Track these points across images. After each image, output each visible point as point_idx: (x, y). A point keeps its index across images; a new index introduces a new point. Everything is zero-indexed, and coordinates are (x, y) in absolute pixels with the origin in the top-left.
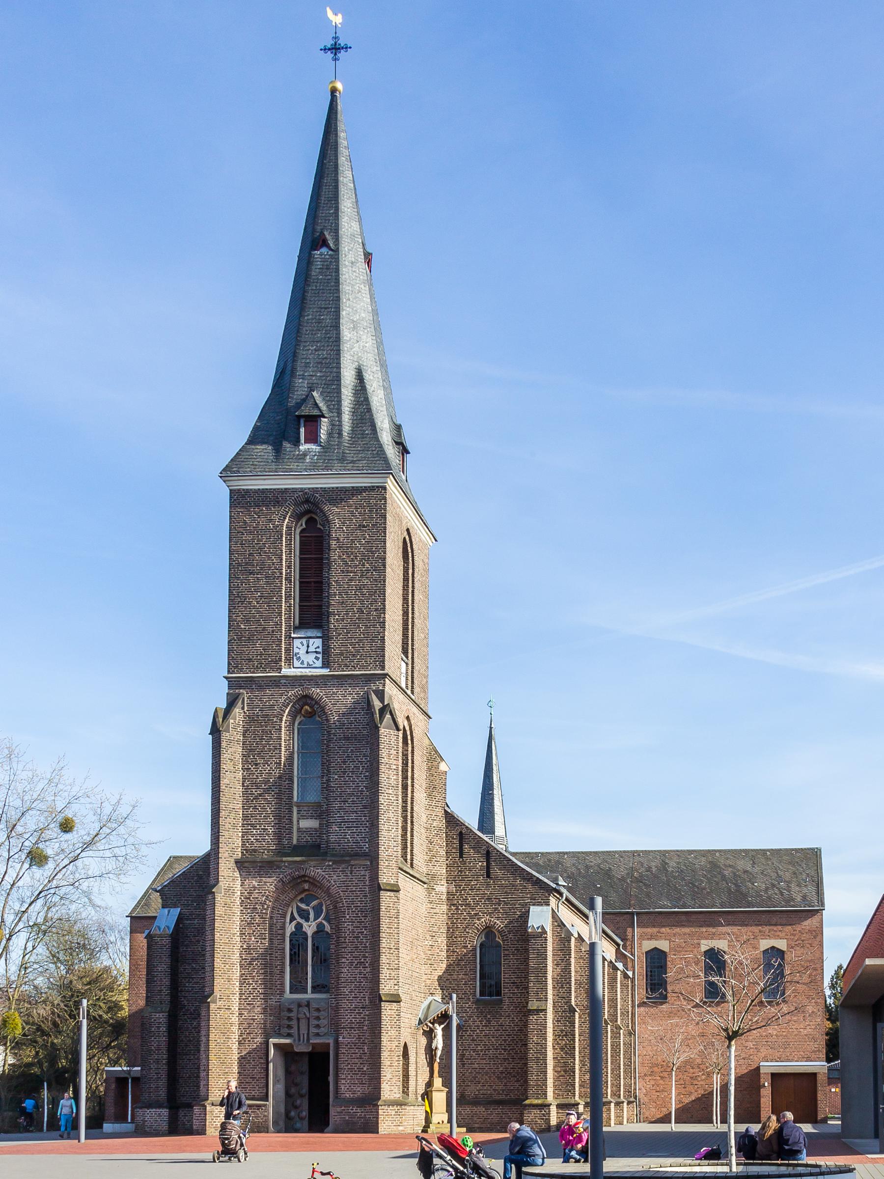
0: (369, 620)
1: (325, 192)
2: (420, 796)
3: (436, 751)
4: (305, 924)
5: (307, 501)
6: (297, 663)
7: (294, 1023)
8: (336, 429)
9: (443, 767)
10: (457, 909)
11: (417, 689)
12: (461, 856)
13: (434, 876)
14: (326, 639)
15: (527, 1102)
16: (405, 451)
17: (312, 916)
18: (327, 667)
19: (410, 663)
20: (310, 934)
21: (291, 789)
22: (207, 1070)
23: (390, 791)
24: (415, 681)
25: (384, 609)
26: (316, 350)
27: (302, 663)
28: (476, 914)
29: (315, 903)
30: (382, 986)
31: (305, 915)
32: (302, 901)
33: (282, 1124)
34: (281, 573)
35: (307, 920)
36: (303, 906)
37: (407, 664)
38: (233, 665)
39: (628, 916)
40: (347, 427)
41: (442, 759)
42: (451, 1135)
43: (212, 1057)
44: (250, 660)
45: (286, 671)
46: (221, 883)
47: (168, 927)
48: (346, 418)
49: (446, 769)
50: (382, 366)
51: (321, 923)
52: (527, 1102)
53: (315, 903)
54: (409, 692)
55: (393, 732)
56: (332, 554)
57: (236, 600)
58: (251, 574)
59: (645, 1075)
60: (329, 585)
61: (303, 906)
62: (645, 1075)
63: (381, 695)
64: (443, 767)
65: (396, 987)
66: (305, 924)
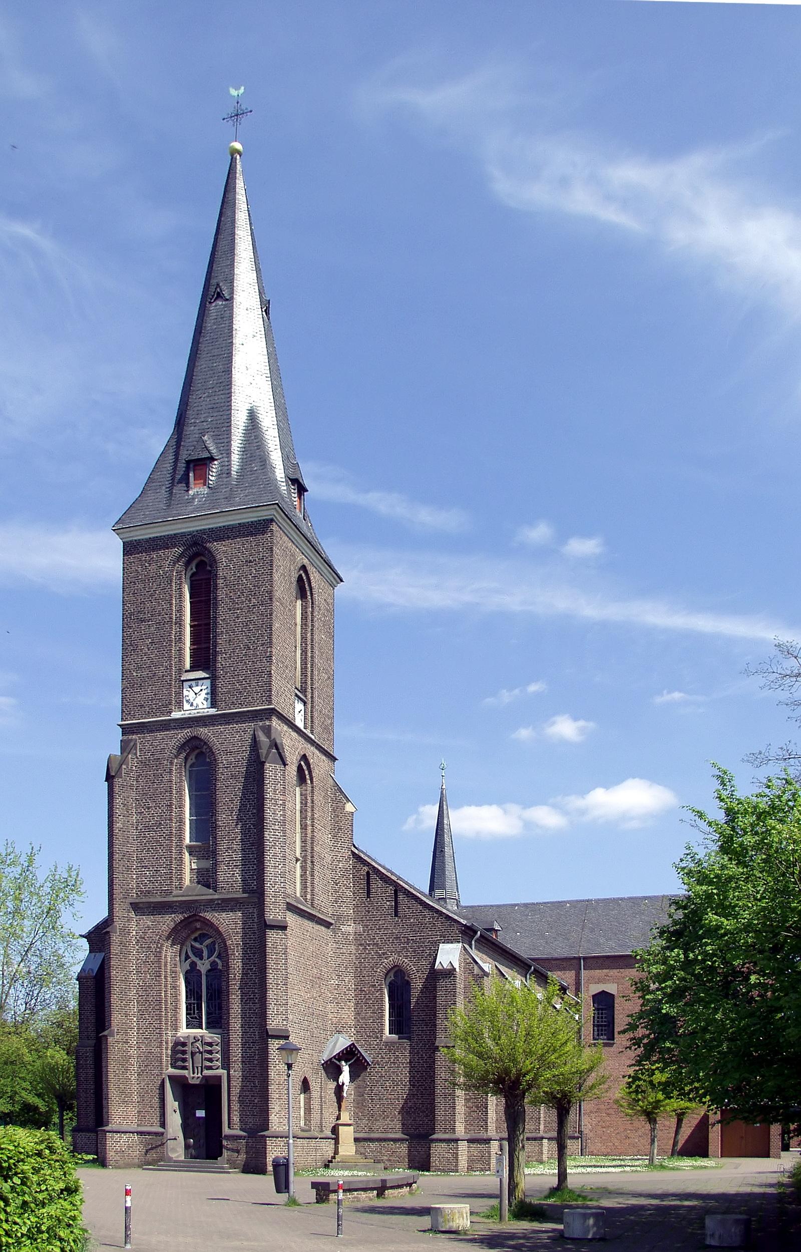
0: (255, 655)
1: (222, 244)
2: (324, 837)
3: (342, 792)
4: (199, 962)
5: (195, 544)
6: (186, 706)
7: (188, 1056)
8: (226, 471)
9: (349, 808)
10: (365, 949)
11: (317, 729)
12: (368, 897)
13: (339, 918)
14: (213, 679)
15: (435, 1136)
16: (302, 490)
17: (205, 954)
18: (214, 707)
19: (309, 702)
20: (203, 972)
21: (181, 830)
22: (107, 1099)
23: (277, 827)
24: (316, 721)
25: (271, 642)
26: (208, 397)
27: (192, 705)
28: (384, 954)
29: (208, 941)
30: (269, 1022)
31: (199, 954)
32: (195, 940)
33: (203, 1151)
34: (171, 618)
35: (201, 959)
36: (197, 945)
37: (305, 703)
38: (125, 714)
39: (575, 961)
40: (235, 467)
41: (348, 800)
42: (718, 1122)
43: (111, 1086)
44: (142, 706)
45: (176, 715)
46: (115, 923)
47: (92, 970)
48: (235, 458)
49: (353, 810)
50: (201, 333)
51: (214, 961)
52: (435, 1136)
53: (208, 941)
54: (308, 732)
55: (279, 767)
56: (219, 593)
57: (129, 647)
58: (142, 621)
59: (591, 1112)
60: (215, 623)
61: (197, 945)
62: (591, 1112)
63: (268, 731)
64: (349, 808)
65: (285, 1023)
66: (199, 962)
